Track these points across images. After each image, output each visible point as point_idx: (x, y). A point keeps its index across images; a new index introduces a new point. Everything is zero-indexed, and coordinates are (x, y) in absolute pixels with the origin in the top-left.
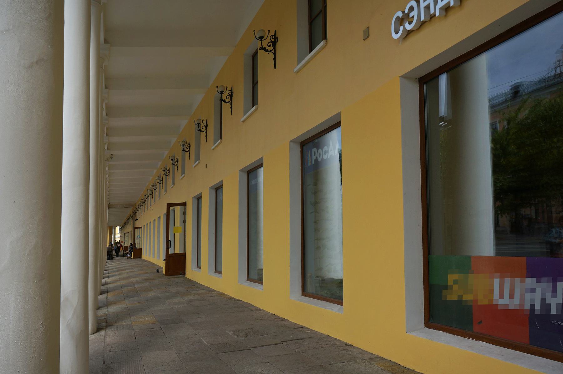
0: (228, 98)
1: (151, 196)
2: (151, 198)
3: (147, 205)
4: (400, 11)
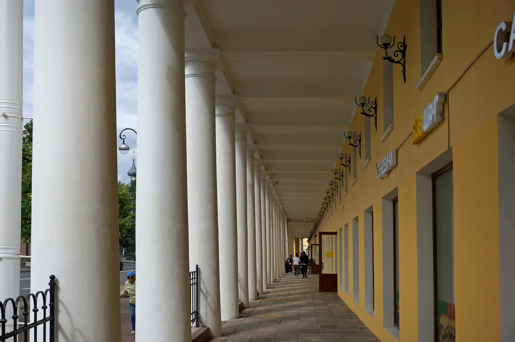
0: (398, 55)
1: (335, 192)
2: (335, 194)
3: (329, 214)
4: (503, 22)
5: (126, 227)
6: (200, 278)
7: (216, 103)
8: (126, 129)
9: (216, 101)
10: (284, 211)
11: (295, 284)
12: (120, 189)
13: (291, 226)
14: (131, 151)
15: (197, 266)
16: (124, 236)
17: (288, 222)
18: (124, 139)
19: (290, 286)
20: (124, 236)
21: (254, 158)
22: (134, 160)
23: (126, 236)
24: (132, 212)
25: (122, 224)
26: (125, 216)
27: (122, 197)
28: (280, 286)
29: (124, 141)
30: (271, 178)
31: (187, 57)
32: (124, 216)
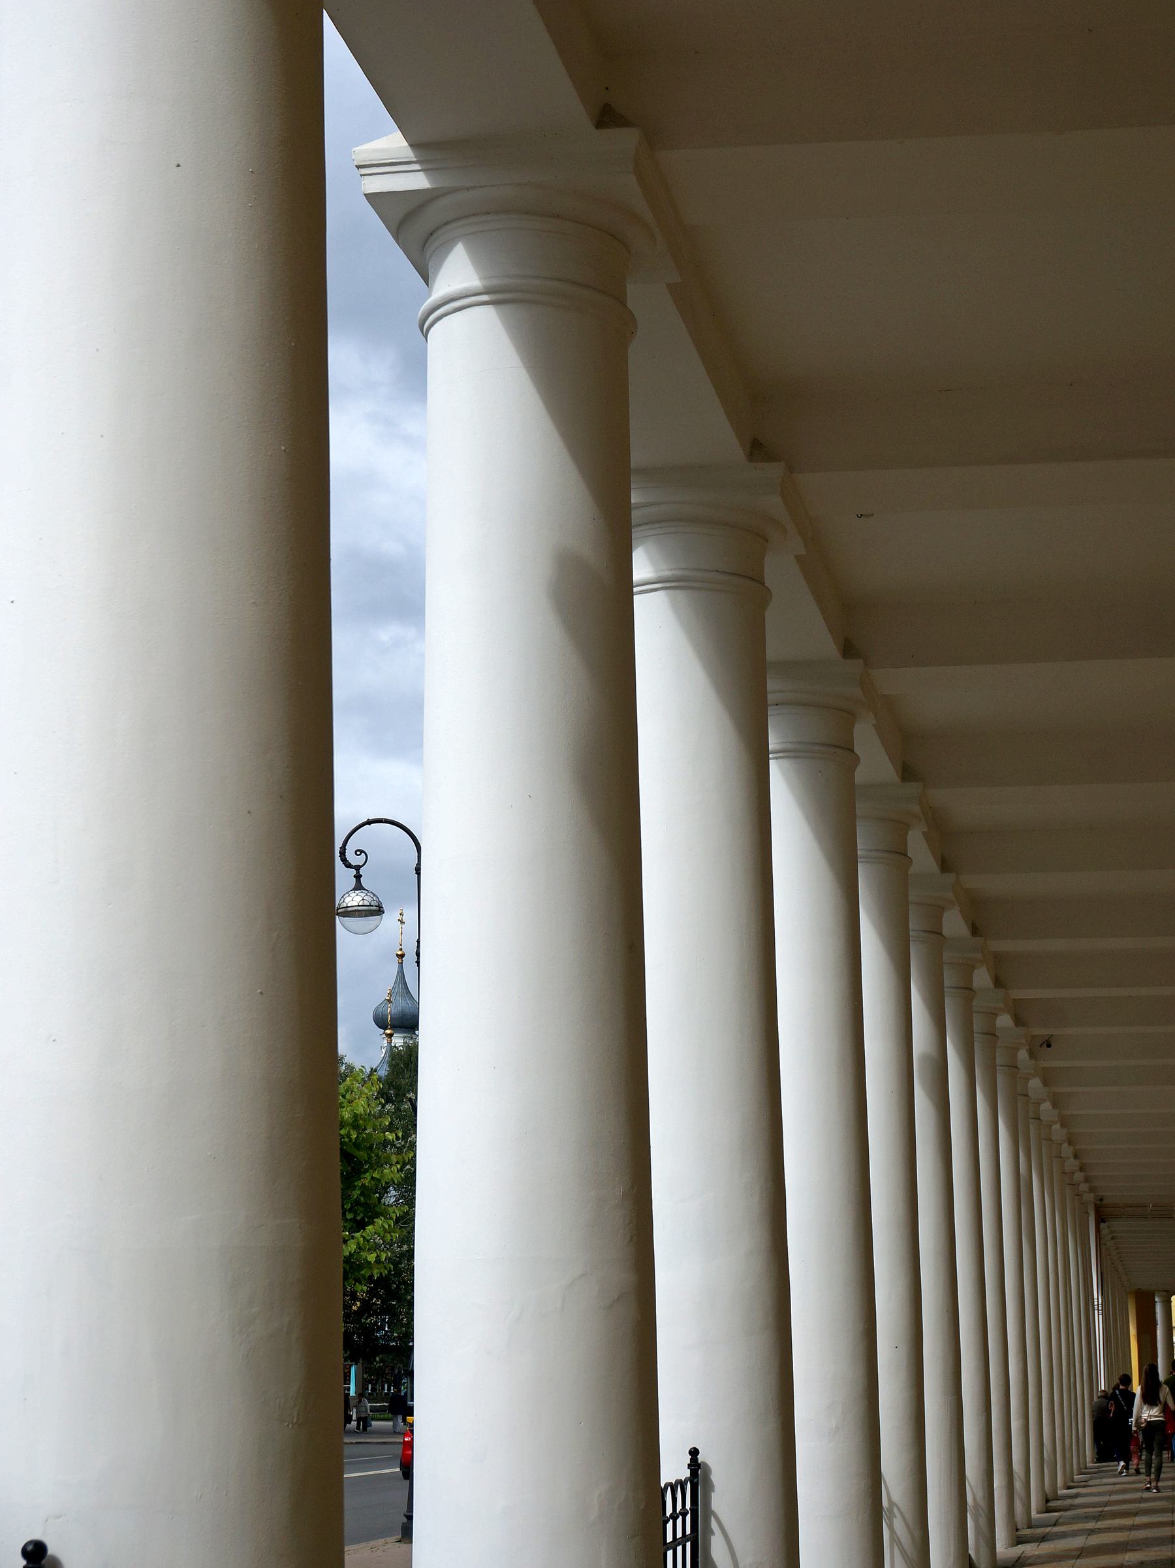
5: (365, 1272)
6: (709, 1513)
7: (771, 698)
8: (369, 822)
9: (861, 858)
10: (1081, 1169)
11: (1145, 1519)
12: (344, 1097)
13: (1113, 1238)
14: (389, 920)
15: (694, 1453)
16: (354, 1308)
17: (1100, 1220)
18: (358, 868)
19: (1121, 1529)
20: (354, 1308)
21: (944, 936)
22: (402, 956)
23: (367, 1307)
24: (392, 1196)
25: (347, 1260)
26: (363, 1219)
27: (348, 1135)
28: (1076, 1527)
29: (358, 877)
30: (1019, 1021)
31: (640, 506)
32: (359, 1218)
